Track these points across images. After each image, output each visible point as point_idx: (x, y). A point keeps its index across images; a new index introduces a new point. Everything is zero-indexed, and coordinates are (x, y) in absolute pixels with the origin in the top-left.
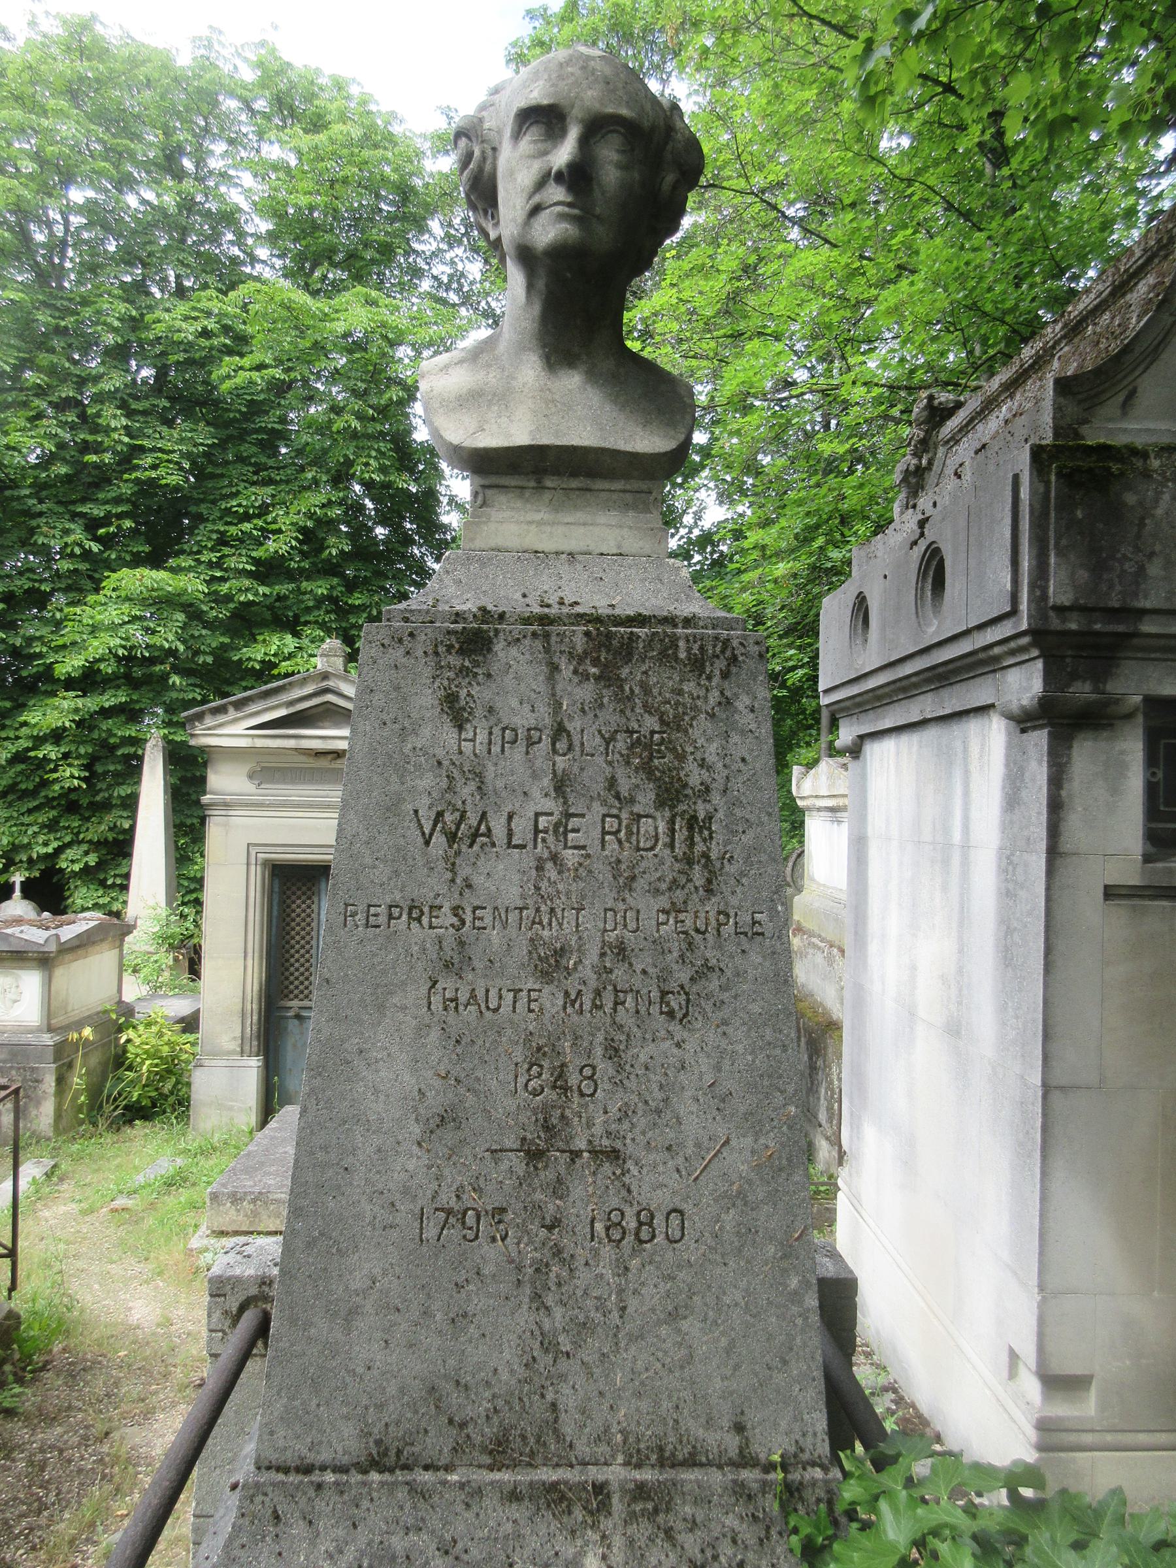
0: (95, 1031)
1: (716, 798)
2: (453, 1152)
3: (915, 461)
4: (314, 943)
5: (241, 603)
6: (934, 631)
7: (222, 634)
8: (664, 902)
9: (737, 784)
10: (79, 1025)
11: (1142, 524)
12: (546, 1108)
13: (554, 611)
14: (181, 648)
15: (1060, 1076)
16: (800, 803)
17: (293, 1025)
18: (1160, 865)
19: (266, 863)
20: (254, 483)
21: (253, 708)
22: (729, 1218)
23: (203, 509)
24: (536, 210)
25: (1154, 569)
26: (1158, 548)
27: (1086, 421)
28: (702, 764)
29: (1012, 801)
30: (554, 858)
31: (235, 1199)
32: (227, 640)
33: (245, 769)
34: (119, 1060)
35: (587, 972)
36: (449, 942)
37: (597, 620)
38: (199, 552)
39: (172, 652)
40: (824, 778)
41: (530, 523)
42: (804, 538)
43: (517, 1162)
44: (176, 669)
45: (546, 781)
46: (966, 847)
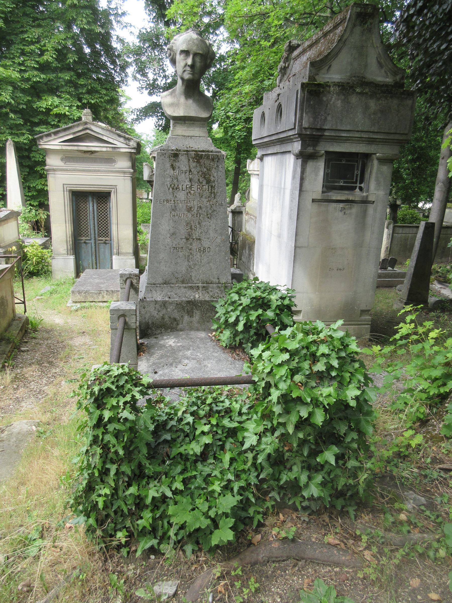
0: (17, 248)
1: (216, 183)
2: (175, 239)
3: (284, 65)
4: (88, 218)
5: (34, 82)
6: (279, 129)
7: (28, 96)
8: (207, 200)
9: (219, 180)
10: (10, 245)
11: (327, 106)
12: (189, 232)
13: (188, 149)
14: (13, 102)
15: (299, 244)
16: (249, 172)
17: (83, 245)
18: (326, 194)
19: (70, 191)
20: (33, 27)
21: (61, 135)
22: (217, 249)
23: (13, 37)
24: (184, 71)
25: (329, 118)
26: (330, 112)
27: (318, 74)
28: (214, 177)
29: (294, 177)
30: (190, 192)
31: (79, 292)
32: (30, 99)
33: (60, 157)
34: (24, 258)
35: (195, 211)
36: (173, 206)
37: (196, 151)
38: (14, 58)
39: (9, 103)
40: (256, 165)
42: (256, 75)
43: (184, 240)
44: (12, 111)
45: (188, 179)
46: (284, 189)
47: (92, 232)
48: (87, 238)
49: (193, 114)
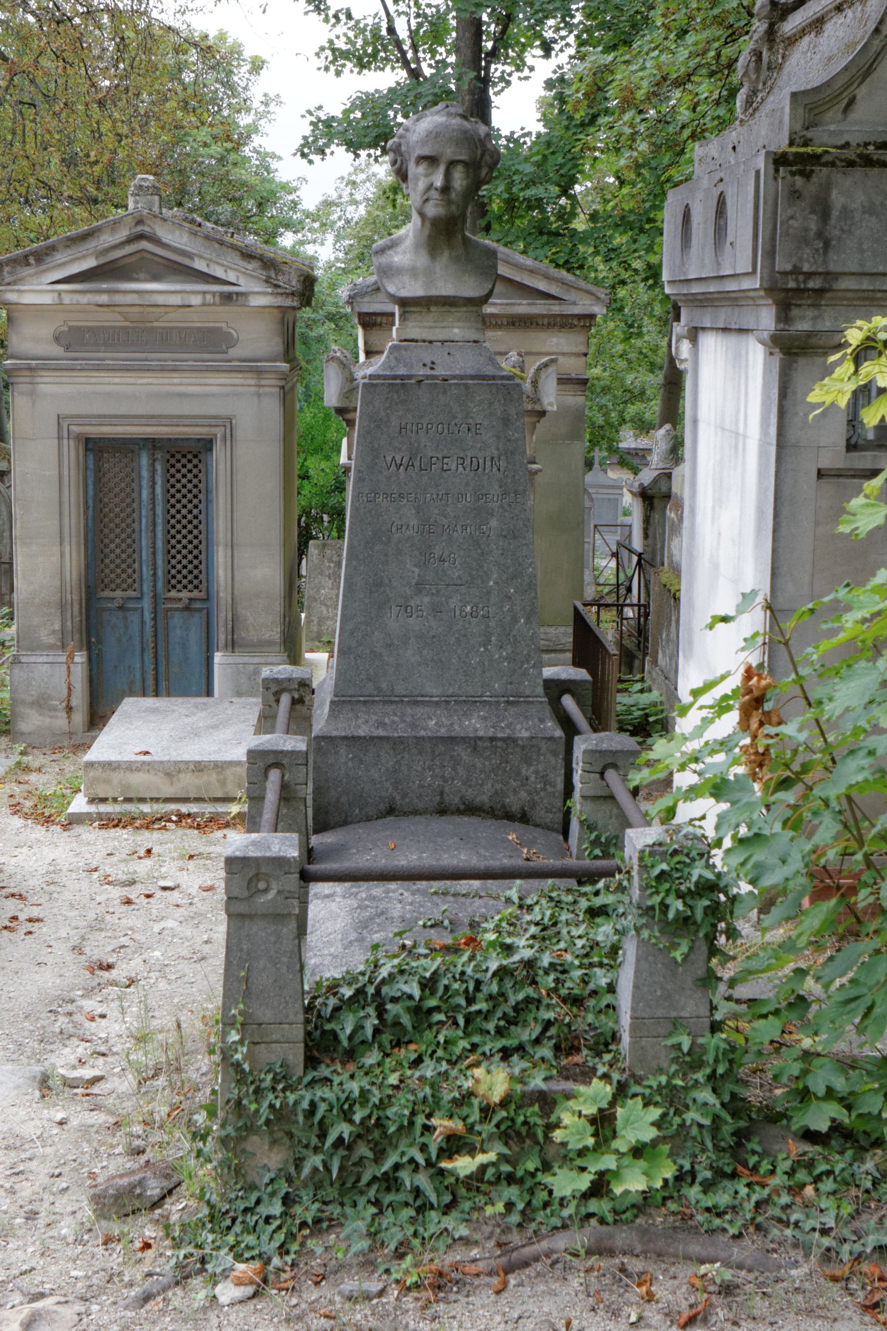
19: (78, 437)
41: (425, 327)
47: (146, 572)
48: (131, 593)
49: (446, 288)
